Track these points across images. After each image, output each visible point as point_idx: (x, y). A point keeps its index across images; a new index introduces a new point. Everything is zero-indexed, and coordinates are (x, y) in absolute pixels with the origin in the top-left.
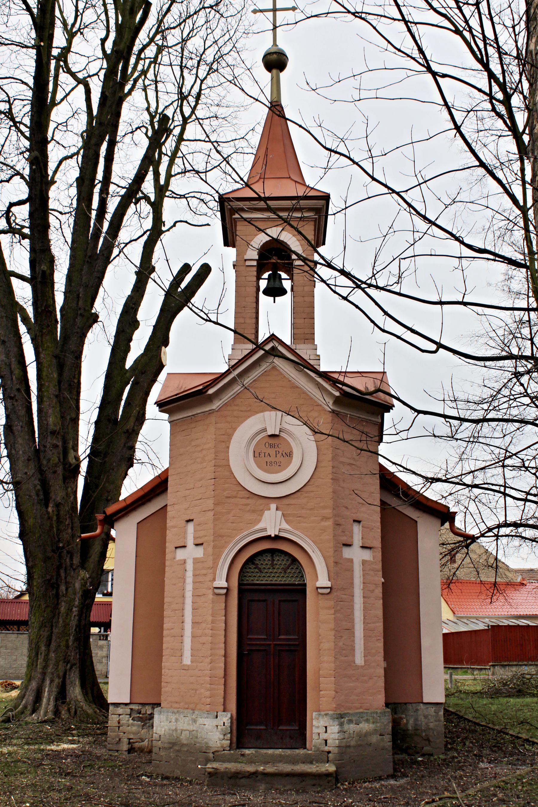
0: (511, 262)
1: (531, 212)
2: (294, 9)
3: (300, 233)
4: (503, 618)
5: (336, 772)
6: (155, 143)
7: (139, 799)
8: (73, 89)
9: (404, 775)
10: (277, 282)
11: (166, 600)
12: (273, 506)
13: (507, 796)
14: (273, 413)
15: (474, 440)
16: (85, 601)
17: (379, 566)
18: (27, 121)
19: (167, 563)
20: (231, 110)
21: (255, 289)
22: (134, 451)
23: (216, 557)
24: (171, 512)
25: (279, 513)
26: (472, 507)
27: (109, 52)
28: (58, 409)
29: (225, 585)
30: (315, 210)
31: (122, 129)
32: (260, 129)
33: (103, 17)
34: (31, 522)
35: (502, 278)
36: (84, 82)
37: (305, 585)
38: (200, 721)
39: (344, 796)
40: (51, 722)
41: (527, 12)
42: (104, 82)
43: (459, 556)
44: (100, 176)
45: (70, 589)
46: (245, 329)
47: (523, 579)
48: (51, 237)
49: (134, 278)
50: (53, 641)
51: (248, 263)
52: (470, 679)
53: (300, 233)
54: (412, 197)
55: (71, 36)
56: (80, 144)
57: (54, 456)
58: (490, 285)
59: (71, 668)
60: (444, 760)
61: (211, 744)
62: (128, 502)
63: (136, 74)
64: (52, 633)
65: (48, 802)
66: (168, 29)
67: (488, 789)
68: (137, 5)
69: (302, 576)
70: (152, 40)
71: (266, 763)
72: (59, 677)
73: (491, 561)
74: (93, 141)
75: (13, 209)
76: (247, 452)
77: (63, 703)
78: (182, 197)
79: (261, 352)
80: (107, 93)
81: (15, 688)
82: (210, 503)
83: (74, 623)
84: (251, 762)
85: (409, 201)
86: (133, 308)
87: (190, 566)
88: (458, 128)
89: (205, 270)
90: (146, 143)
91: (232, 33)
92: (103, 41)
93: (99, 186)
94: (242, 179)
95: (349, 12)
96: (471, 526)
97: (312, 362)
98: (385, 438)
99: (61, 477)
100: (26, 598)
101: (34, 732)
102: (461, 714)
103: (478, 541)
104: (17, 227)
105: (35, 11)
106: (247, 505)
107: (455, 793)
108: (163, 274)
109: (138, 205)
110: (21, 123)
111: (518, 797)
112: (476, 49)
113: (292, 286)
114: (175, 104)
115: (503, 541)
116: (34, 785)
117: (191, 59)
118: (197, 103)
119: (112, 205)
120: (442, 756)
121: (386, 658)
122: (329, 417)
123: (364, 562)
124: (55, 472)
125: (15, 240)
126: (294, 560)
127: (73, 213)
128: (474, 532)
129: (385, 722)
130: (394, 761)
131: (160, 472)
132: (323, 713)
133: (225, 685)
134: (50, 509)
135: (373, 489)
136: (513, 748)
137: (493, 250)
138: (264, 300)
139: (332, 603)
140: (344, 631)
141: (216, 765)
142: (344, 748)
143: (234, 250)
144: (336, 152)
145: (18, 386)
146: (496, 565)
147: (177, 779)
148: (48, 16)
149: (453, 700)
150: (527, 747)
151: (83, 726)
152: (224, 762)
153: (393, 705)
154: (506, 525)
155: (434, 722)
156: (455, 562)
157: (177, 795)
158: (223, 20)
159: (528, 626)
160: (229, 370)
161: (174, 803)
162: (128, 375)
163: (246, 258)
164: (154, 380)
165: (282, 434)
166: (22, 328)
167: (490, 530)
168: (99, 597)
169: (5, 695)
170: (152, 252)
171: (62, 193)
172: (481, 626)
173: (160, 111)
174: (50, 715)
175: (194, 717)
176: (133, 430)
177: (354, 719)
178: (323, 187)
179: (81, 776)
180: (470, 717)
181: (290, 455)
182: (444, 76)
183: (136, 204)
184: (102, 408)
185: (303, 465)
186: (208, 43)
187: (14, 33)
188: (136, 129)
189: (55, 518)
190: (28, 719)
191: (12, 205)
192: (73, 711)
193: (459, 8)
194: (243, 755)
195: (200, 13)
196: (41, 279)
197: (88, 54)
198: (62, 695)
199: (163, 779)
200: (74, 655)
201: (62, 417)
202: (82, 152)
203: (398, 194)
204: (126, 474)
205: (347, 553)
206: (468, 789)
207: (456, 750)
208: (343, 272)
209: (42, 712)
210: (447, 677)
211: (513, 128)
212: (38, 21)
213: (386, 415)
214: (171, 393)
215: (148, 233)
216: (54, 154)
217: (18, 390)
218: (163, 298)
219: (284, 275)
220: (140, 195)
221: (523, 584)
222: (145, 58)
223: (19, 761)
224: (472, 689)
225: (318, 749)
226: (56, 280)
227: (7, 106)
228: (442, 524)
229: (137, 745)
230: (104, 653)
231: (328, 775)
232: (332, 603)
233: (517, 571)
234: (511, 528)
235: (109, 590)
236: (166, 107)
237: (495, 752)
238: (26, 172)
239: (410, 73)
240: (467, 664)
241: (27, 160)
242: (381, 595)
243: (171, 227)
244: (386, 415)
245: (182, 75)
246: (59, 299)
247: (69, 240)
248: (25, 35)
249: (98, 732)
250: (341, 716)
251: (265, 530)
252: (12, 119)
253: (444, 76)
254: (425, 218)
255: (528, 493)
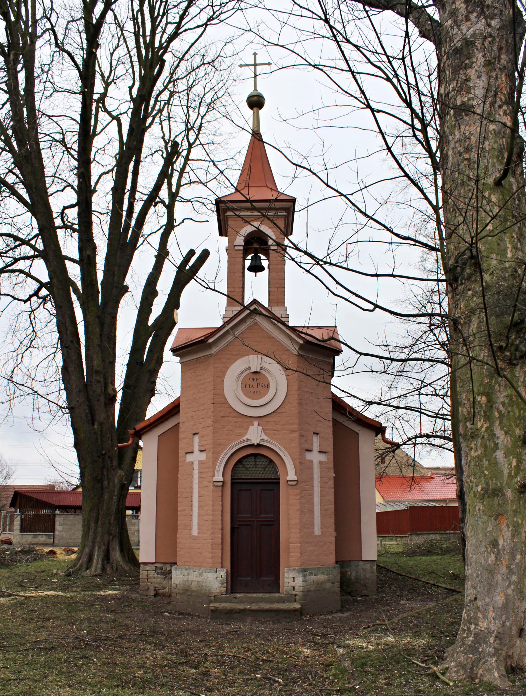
0: (426, 246)
1: (441, 211)
2: (269, 64)
3: (275, 224)
4: (417, 501)
5: (301, 608)
6: (169, 162)
7: (163, 628)
8: (108, 124)
9: (348, 610)
10: (258, 262)
11: (179, 490)
12: (256, 423)
13: (420, 622)
14: (255, 356)
15: (398, 374)
16: (122, 491)
17: (332, 465)
18: (76, 147)
19: (180, 464)
20: (224, 137)
21: (242, 267)
22: (155, 385)
23: (215, 460)
24: (182, 428)
25: (260, 428)
26: (397, 424)
27: (134, 96)
28: (100, 355)
29: (221, 479)
30: (284, 210)
31: (145, 152)
32: (245, 152)
33: (130, 71)
34: (82, 436)
35: (419, 260)
36: (117, 118)
37: (279, 479)
38: (205, 574)
39: (307, 625)
40: (100, 576)
41: (439, 66)
42: (131, 118)
43: (388, 459)
44: (129, 186)
45: (111, 484)
46: (235, 295)
47: (432, 474)
48: (93, 231)
49: (154, 260)
50: (100, 519)
51: (237, 248)
52: (394, 544)
53: (275, 224)
54: (356, 199)
55: (107, 85)
56: (114, 163)
57: (98, 390)
58: (410, 265)
59: (113, 538)
60: (377, 599)
61: (213, 590)
62: (152, 421)
63: (155, 112)
64: (99, 514)
65: (99, 630)
66: (178, 79)
67: (406, 618)
68: (155, 62)
69: (277, 473)
70: (166, 88)
71: (252, 603)
72: (104, 545)
73: (410, 461)
74: (124, 161)
75: (66, 211)
76: (237, 384)
77: (108, 563)
78: (189, 201)
79: (248, 312)
80: (134, 126)
81: (74, 552)
82: (210, 421)
83: (114, 507)
84: (241, 602)
85: (354, 202)
86: (153, 282)
87: (196, 467)
88: (389, 149)
89: (205, 254)
90: (162, 162)
91: (224, 81)
92: (131, 88)
93: (128, 194)
94: (232, 185)
95: (310, 65)
96: (396, 437)
97: (283, 320)
98: (336, 373)
99: (103, 404)
100: (80, 490)
101: (88, 583)
102: (388, 568)
103: (402, 447)
104: (69, 224)
105: (81, 67)
106: (236, 422)
107: (384, 621)
108: (176, 256)
109: (157, 207)
110: (71, 148)
111: (427, 623)
112: (402, 92)
113: (269, 265)
114: (183, 134)
115: (419, 447)
116: (89, 619)
117: (195, 101)
118: (199, 133)
119: (138, 207)
120: (375, 597)
121: (336, 530)
122: (296, 359)
123: (321, 463)
124: (99, 400)
125: (67, 234)
126: (271, 461)
127: (110, 214)
128: (399, 441)
129: (336, 575)
130: (341, 601)
131: (174, 399)
132: (292, 568)
133: (222, 549)
134: (95, 427)
135: (328, 406)
136: (424, 590)
137: (414, 238)
138: (249, 275)
139: (298, 491)
140: (307, 511)
141: (216, 605)
142: (306, 592)
143: (227, 238)
144: (301, 166)
145: (71, 339)
146: (413, 465)
147: (189, 614)
148: (90, 70)
149: (383, 559)
150: (434, 589)
151: (122, 578)
152: (222, 602)
153: (342, 563)
154: (421, 436)
155: (370, 574)
156: (384, 462)
157: (189, 625)
158: (217, 72)
159: (435, 507)
160: (223, 325)
161: (187, 631)
162: (150, 330)
163: (235, 244)
164: (169, 334)
165: (262, 371)
166: (74, 297)
167: (410, 439)
168: (131, 489)
169: (67, 557)
170: (167, 241)
171: (101, 199)
172: (402, 507)
173: (172, 139)
174: (99, 571)
175: (200, 572)
176: (155, 370)
177: (313, 572)
178: (290, 192)
179: (122, 613)
180: (394, 570)
181: (267, 386)
182: (379, 111)
183: (155, 206)
184: (132, 354)
185: (277, 394)
186: (207, 90)
187: (66, 83)
188: (155, 152)
189: (99, 433)
190: (84, 574)
191: (65, 208)
192: (115, 568)
193: (390, 62)
194: (235, 598)
195: (201, 68)
196: (87, 260)
197: (120, 98)
198: (107, 557)
199: (179, 614)
200: (115, 530)
201: (103, 361)
202: (115, 169)
203: (345, 196)
204: (150, 401)
205: (309, 456)
206: (393, 618)
207: (385, 592)
208: (306, 253)
209: (93, 569)
210: (379, 543)
211: (428, 149)
212: (83, 73)
213: (336, 357)
214: (182, 342)
215: (164, 227)
216: (95, 170)
217: (72, 341)
218: (174, 274)
219: (262, 257)
220: (158, 200)
221: (432, 478)
222: (161, 101)
223: (78, 602)
224: (396, 550)
225: (288, 593)
226: (97, 261)
227: (62, 137)
228: (376, 436)
229: (160, 591)
230: (136, 528)
231: (295, 610)
232: (298, 491)
233: (427, 469)
234: (424, 438)
235: (139, 484)
236: (177, 136)
237: (411, 593)
238: (76, 184)
239: (354, 109)
240: (393, 533)
241: (76, 175)
242: (333, 486)
243: (181, 223)
244: (336, 357)
245: (188, 112)
246: (100, 276)
247: (107, 233)
248: (74, 84)
249: (133, 582)
250: (304, 570)
251: (250, 440)
252: (65, 146)
253: (379, 111)
254: (365, 214)
255: (438, 414)
